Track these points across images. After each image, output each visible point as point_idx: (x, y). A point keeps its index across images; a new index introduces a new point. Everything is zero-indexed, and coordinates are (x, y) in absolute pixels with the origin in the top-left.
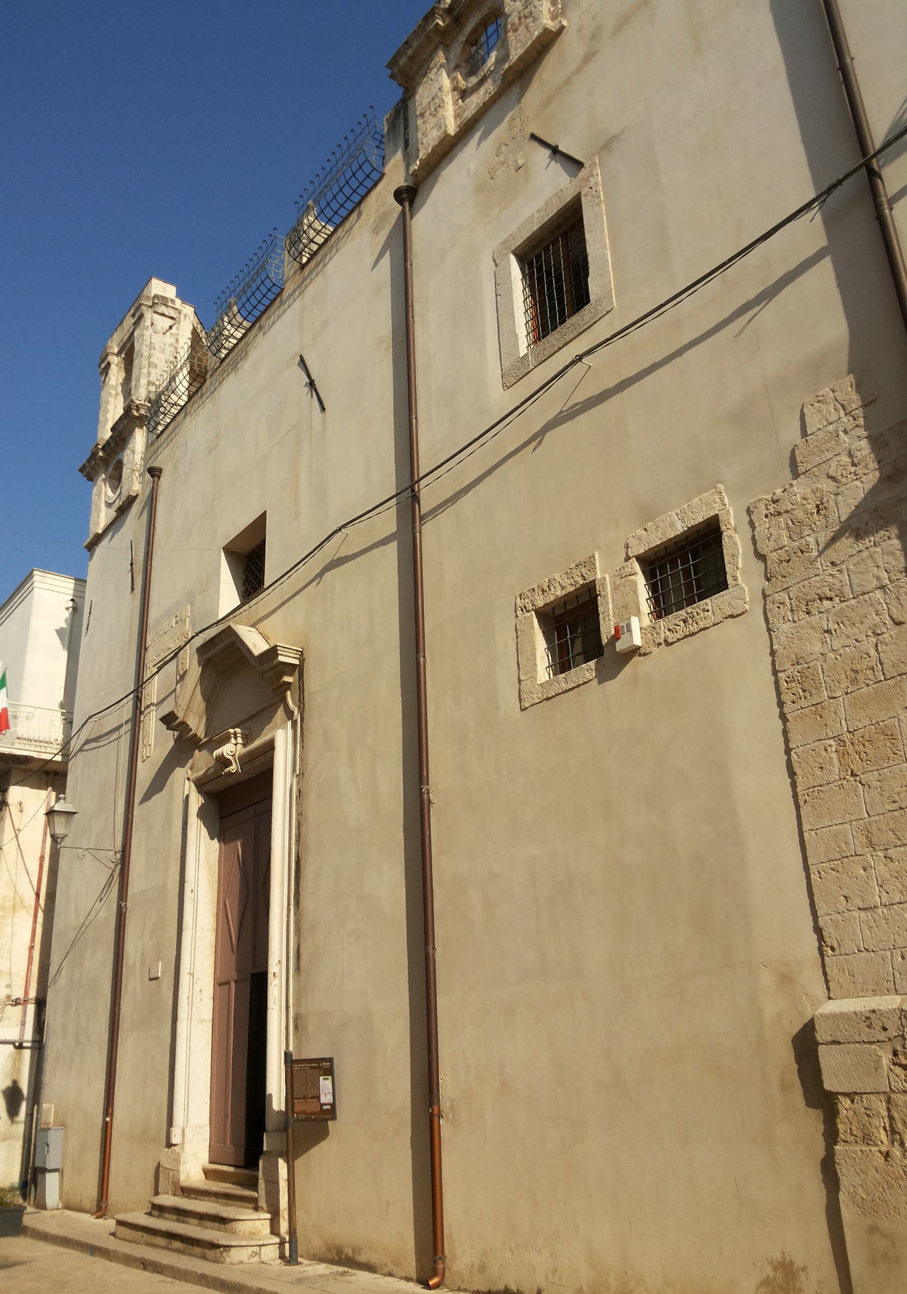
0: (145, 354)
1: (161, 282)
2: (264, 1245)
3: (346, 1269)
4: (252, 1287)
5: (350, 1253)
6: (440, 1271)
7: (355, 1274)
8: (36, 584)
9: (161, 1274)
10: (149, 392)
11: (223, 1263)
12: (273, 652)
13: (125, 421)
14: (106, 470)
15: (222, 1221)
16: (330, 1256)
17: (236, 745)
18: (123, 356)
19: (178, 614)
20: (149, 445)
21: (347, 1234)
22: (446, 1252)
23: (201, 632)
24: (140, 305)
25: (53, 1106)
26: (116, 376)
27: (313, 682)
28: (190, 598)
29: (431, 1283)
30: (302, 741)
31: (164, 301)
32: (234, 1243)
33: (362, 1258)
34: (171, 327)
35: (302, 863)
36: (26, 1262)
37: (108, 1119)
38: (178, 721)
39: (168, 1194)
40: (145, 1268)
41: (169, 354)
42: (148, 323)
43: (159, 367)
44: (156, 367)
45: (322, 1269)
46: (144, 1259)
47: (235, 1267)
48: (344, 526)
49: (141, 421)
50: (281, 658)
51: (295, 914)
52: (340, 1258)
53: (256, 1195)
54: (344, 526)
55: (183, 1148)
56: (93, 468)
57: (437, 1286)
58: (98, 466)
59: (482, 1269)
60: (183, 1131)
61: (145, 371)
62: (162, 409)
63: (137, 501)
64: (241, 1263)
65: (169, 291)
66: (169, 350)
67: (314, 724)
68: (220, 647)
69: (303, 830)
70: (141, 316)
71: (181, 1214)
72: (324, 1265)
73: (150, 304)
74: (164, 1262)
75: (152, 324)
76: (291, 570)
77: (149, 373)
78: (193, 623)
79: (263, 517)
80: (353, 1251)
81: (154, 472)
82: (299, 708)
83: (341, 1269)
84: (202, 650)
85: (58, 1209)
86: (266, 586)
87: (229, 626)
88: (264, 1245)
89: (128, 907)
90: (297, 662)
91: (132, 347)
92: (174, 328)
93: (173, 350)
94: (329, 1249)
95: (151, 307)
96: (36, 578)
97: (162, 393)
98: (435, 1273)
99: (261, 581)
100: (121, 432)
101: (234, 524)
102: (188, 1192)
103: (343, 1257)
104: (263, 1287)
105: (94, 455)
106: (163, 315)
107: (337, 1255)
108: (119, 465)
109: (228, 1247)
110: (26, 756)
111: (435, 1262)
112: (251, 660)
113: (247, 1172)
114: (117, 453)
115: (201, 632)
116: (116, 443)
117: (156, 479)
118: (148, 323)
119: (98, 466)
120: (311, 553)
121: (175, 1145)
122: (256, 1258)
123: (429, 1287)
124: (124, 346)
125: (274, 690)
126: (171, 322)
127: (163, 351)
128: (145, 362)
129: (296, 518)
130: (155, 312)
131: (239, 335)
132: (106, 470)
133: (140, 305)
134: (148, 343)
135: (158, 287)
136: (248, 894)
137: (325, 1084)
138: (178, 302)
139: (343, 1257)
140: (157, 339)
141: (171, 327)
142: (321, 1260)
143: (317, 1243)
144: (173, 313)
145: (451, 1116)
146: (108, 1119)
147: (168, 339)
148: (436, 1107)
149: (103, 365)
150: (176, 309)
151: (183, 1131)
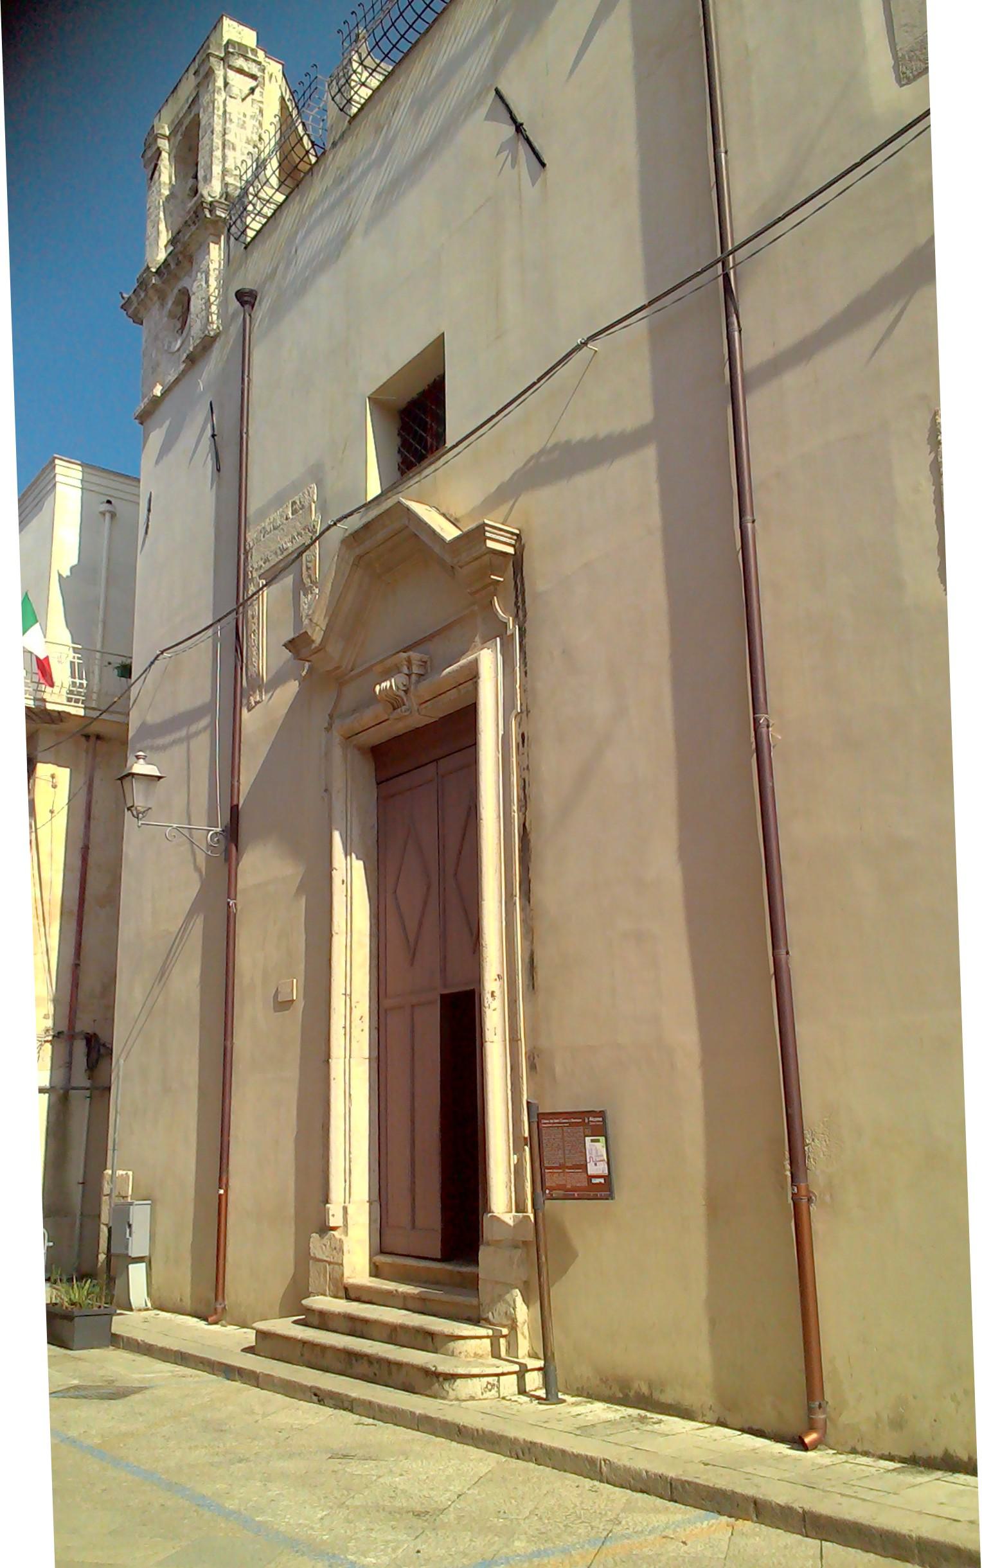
0: (218, 128)
1: (235, 24)
2: (503, 1374)
3: (643, 1413)
4: (516, 1439)
5: (645, 1390)
6: (820, 1424)
7: (660, 1422)
8: (58, 478)
9: (351, 1411)
10: (227, 185)
11: (444, 1398)
12: (478, 534)
13: (193, 228)
14: (162, 305)
15: (429, 1340)
16: (607, 1392)
17: (409, 675)
18: (179, 137)
19: (296, 498)
20: (228, 260)
21: (634, 1361)
22: (827, 1397)
23: (339, 520)
24: (209, 55)
25: (130, 1173)
26: (166, 173)
27: (541, 575)
28: (316, 474)
29: (807, 1440)
30: (524, 662)
31: (243, 51)
32: (461, 1371)
33: (667, 1397)
34: (252, 90)
35: (533, 837)
36: (140, 1390)
37: (222, 1192)
38: (314, 646)
39: (325, 1295)
40: (321, 1402)
41: (250, 132)
42: (220, 83)
43: (238, 148)
44: (234, 149)
45: (599, 1411)
46: (319, 1389)
47: (464, 1404)
48: (592, 338)
49: (218, 227)
50: (490, 544)
51: (522, 909)
52: (626, 1395)
53: (474, 1302)
54: (592, 338)
55: (346, 1233)
56: (141, 302)
57: (814, 1446)
58: (162, 298)
59: (898, 1424)
60: (345, 1209)
61: (218, 154)
62: (250, 208)
63: (217, 345)
64: (472, 1398)
65: (248, 37)
66: (250, 123)
67: (544, 640)
68: (381, 535)
69: (532, 791)
70: (210, 73)
71: (357, 1327)
72: (599, 1406)
73: (222, 55)
74: (354, 1395)
75: (226, 84)
76: (498, 413)
77: (224, 157)
78: (323, 508)
79: (440, 342)
80: (650, 1387)
81: (246, 298)
82: (517, 616)
83: (634, 1412)
84: (355, 538)
85: (147, 1309)
86: (448, 445)
87: (399, 502)
88: (503, 1374)
89: (239, 907)
90: (511, 550)
91: (196, 122)
92: (257, 91)
93: (257, 124)
94: (604, 1381)
95: (222, 59)
96: (58, 469)
97: (250, 183)
98: (811, 1428)
99: (441, 437)
100: (186, 246)
101: (386, 358)
102: (350, 1293)
103: (632, 1394)
104: (538, 1440)
105: (142, 284)
106: (240, 71)
107: (621, 1390)
108: (185, 299)
109: (454, 1377)
110: (59, 712)
111: (810, 1411)
112: (437, 549)
113: (448, 1267)
114: (177, 278)
115: (339, 520)
116: (178, 263)
117: (247, 307)
118: (220, 83)
119: (162, 298)
120: (534, 384)
121: (334, 1229)
122: (493, 1392)
123: (805, 1448)
124: (180, 123)
125: (472, 594)
126: (253, 83)
127: (243, 126)
128: (218, 142)
129: (498, 337)
130: (230, 67)
131: (374, 83)
132: (162, 305)
133: (209, 55)
134: (221, 112)
135: (232, 30)
136: (428, 889)
137: (595, 1149)
138: (261, 55)
139: (632, 1394)
140: (234, 106)
141: (252, 90)
142: (592, 1396)
143: (584, 1372)
144: (254, 70)
145: (828, 1198)
146: (222, 1192)
147: (249, 108)
148: (803, 1185)
149: (149, 154)
150: (259, 63)
151: (345, 1209)
